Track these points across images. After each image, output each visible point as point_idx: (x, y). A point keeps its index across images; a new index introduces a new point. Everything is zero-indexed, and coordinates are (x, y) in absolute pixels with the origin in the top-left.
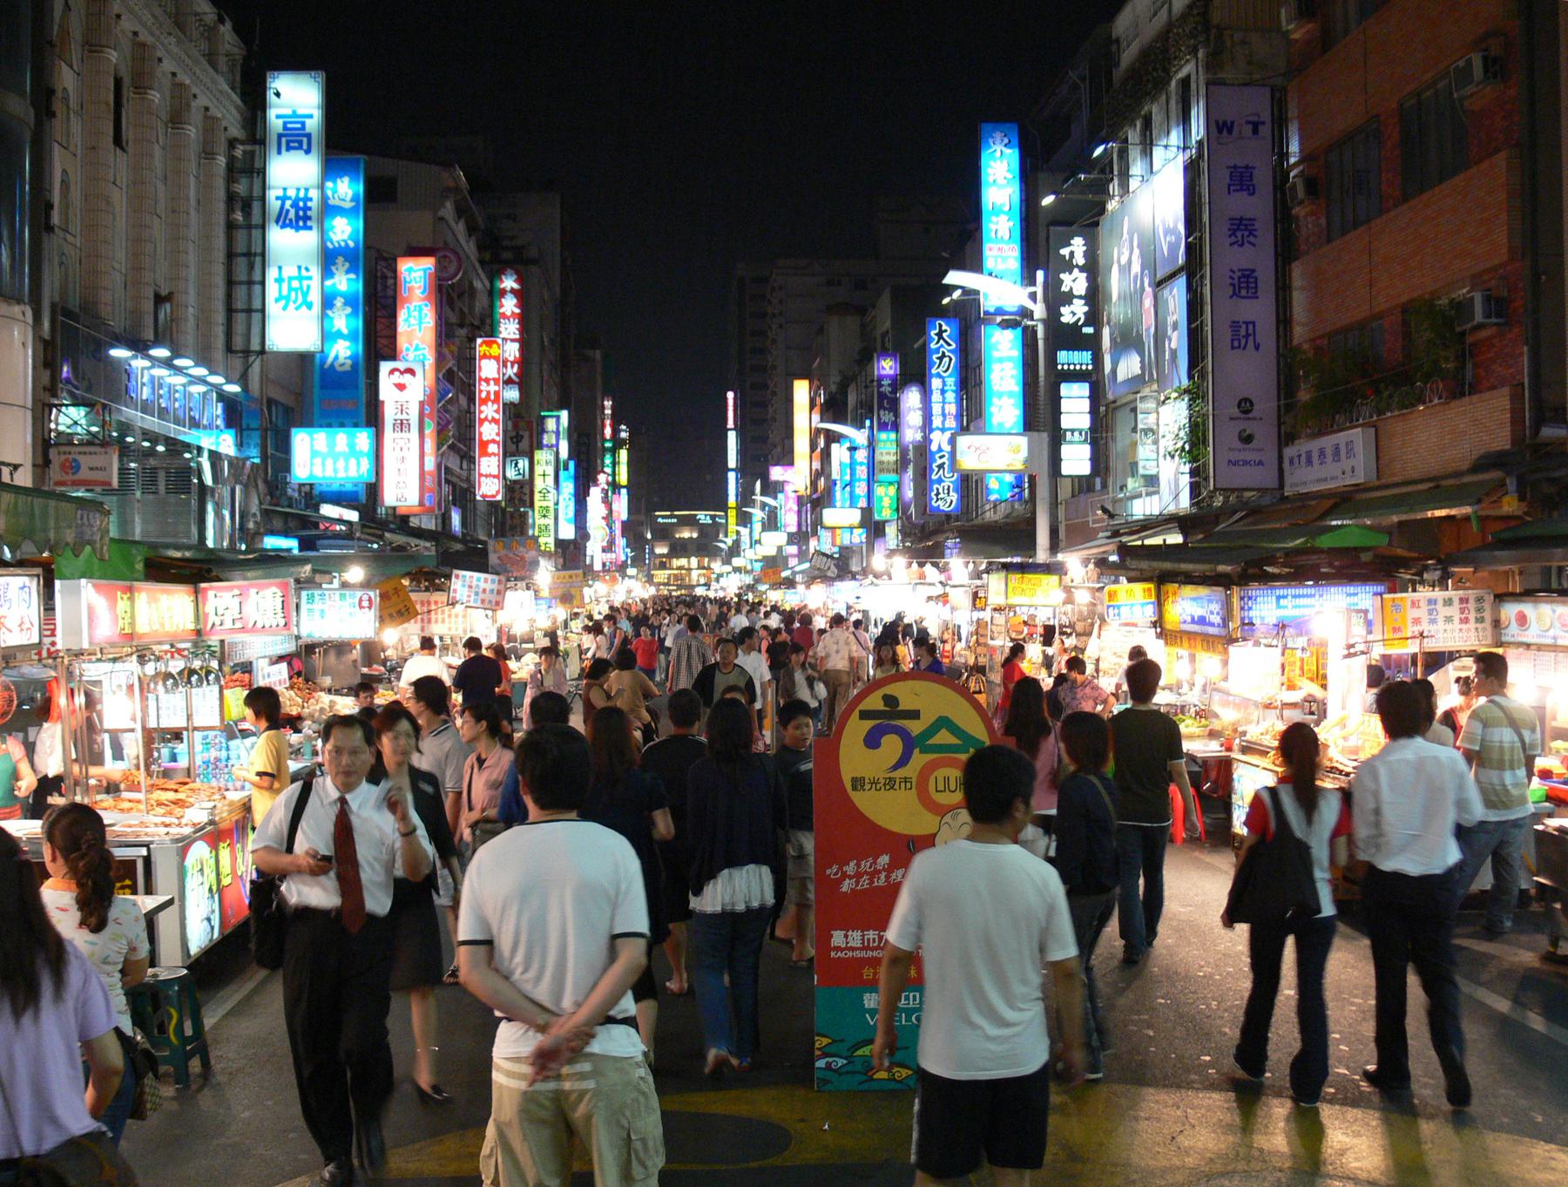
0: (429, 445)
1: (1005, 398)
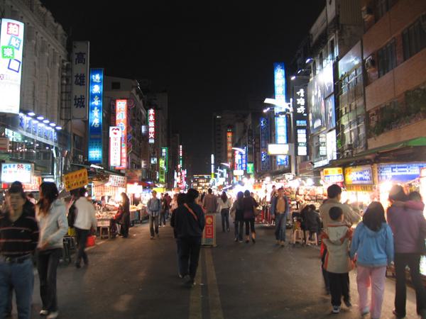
0: (124, 151)
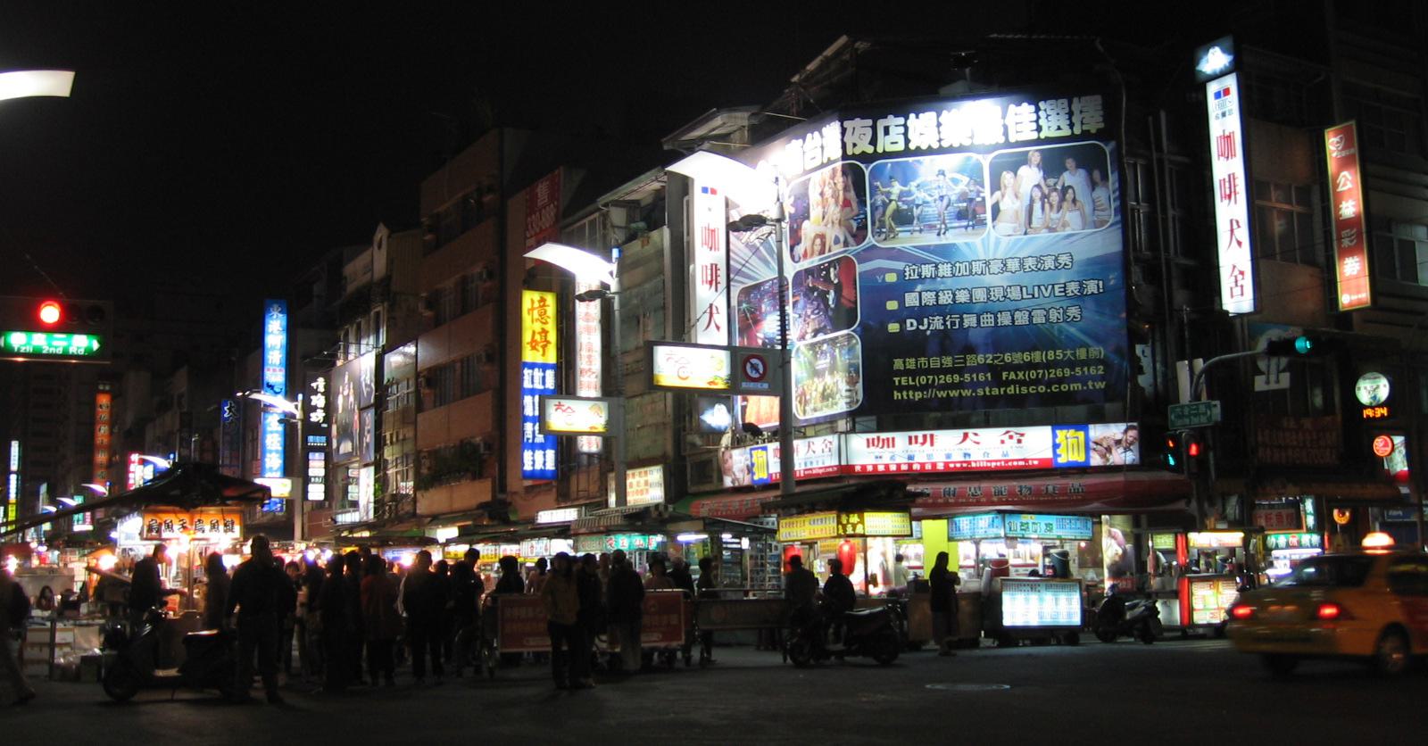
1: (274, 454)
